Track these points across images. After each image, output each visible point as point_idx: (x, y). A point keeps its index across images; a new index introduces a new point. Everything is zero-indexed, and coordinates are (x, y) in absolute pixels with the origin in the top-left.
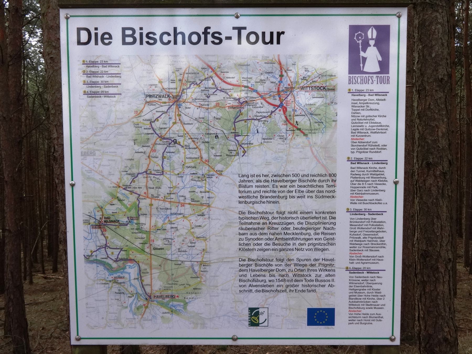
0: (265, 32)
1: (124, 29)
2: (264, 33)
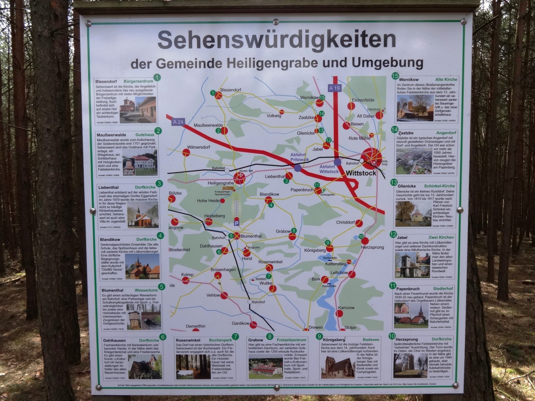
2: (199, 46)
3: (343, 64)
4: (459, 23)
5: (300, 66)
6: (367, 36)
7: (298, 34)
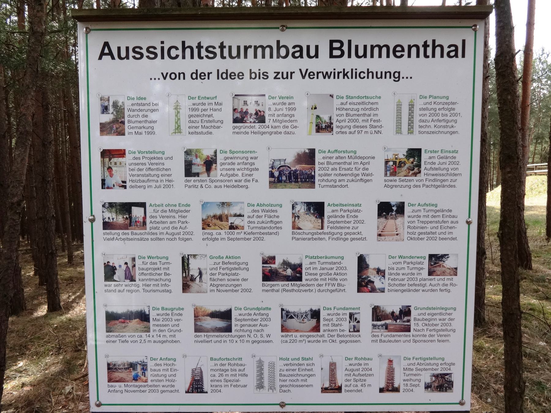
0: (351, 40)
1: (332, 42)
2: (388, 56)
4: (471, 29)
5: (301, 56)
6: (202, 47)
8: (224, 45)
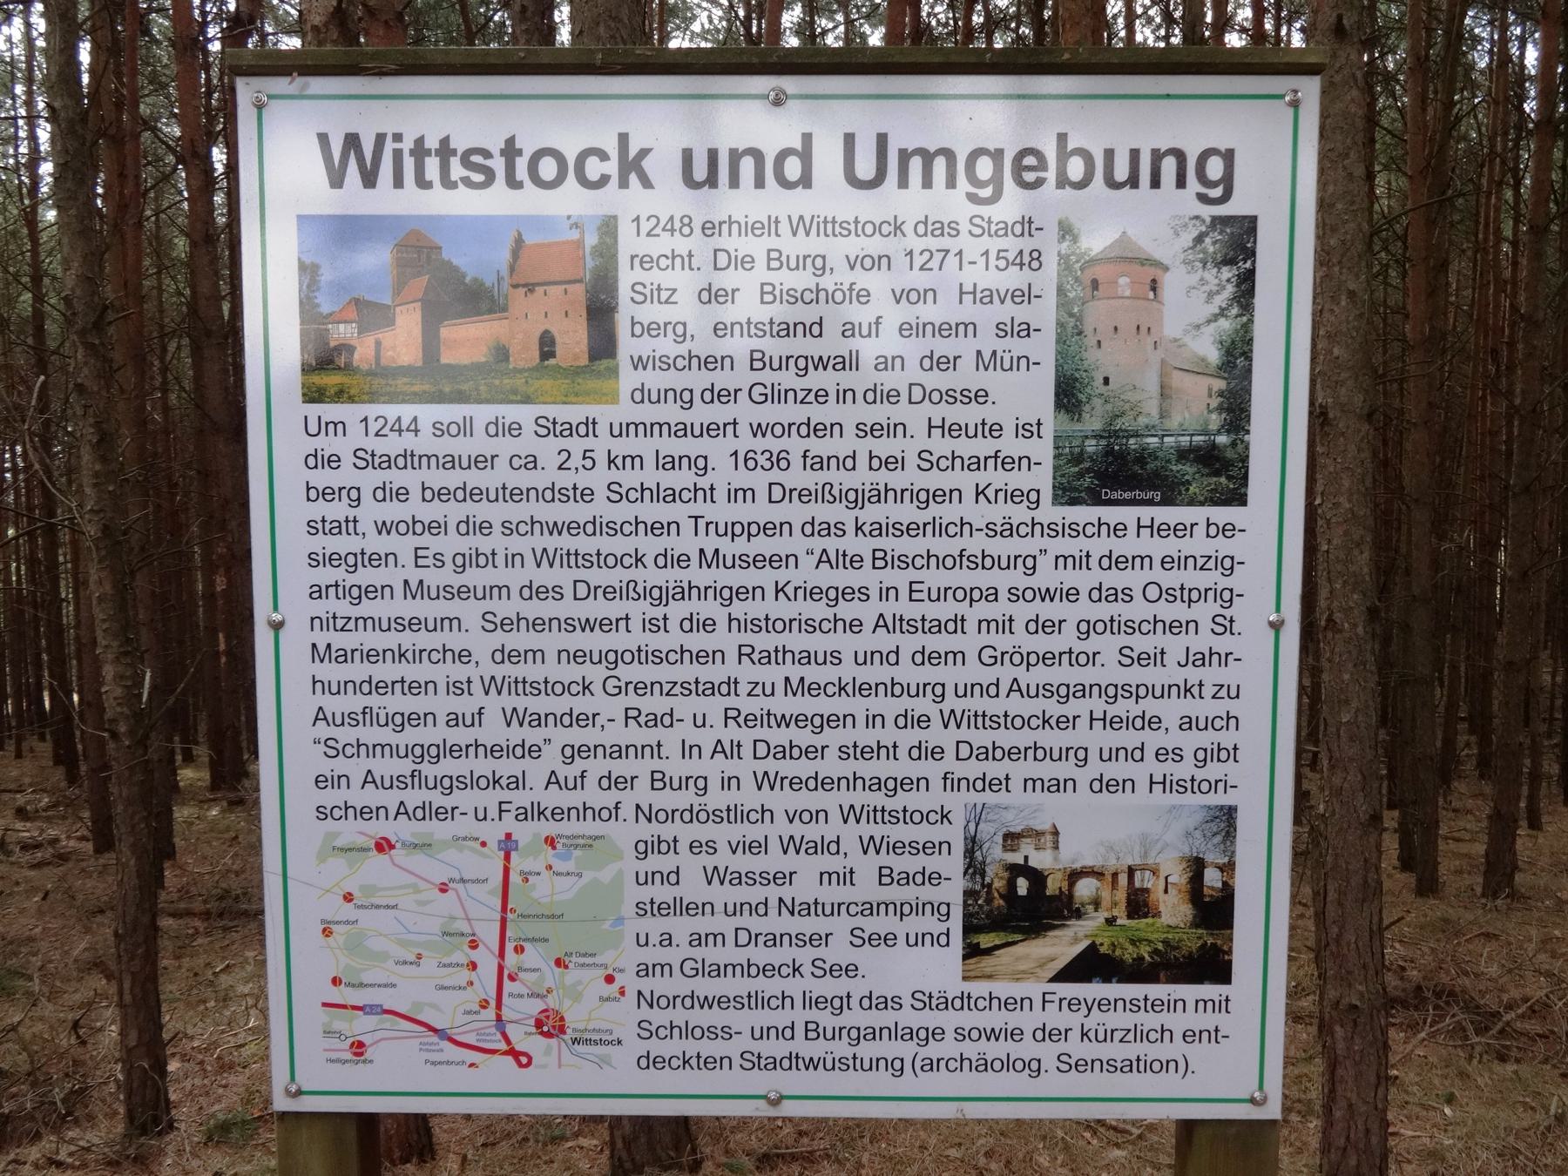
0: (627, 134)
2: (760, 183)
3: (793, 168)
6: (520, 152)
7: (798, 145)
8: (518, 146)
